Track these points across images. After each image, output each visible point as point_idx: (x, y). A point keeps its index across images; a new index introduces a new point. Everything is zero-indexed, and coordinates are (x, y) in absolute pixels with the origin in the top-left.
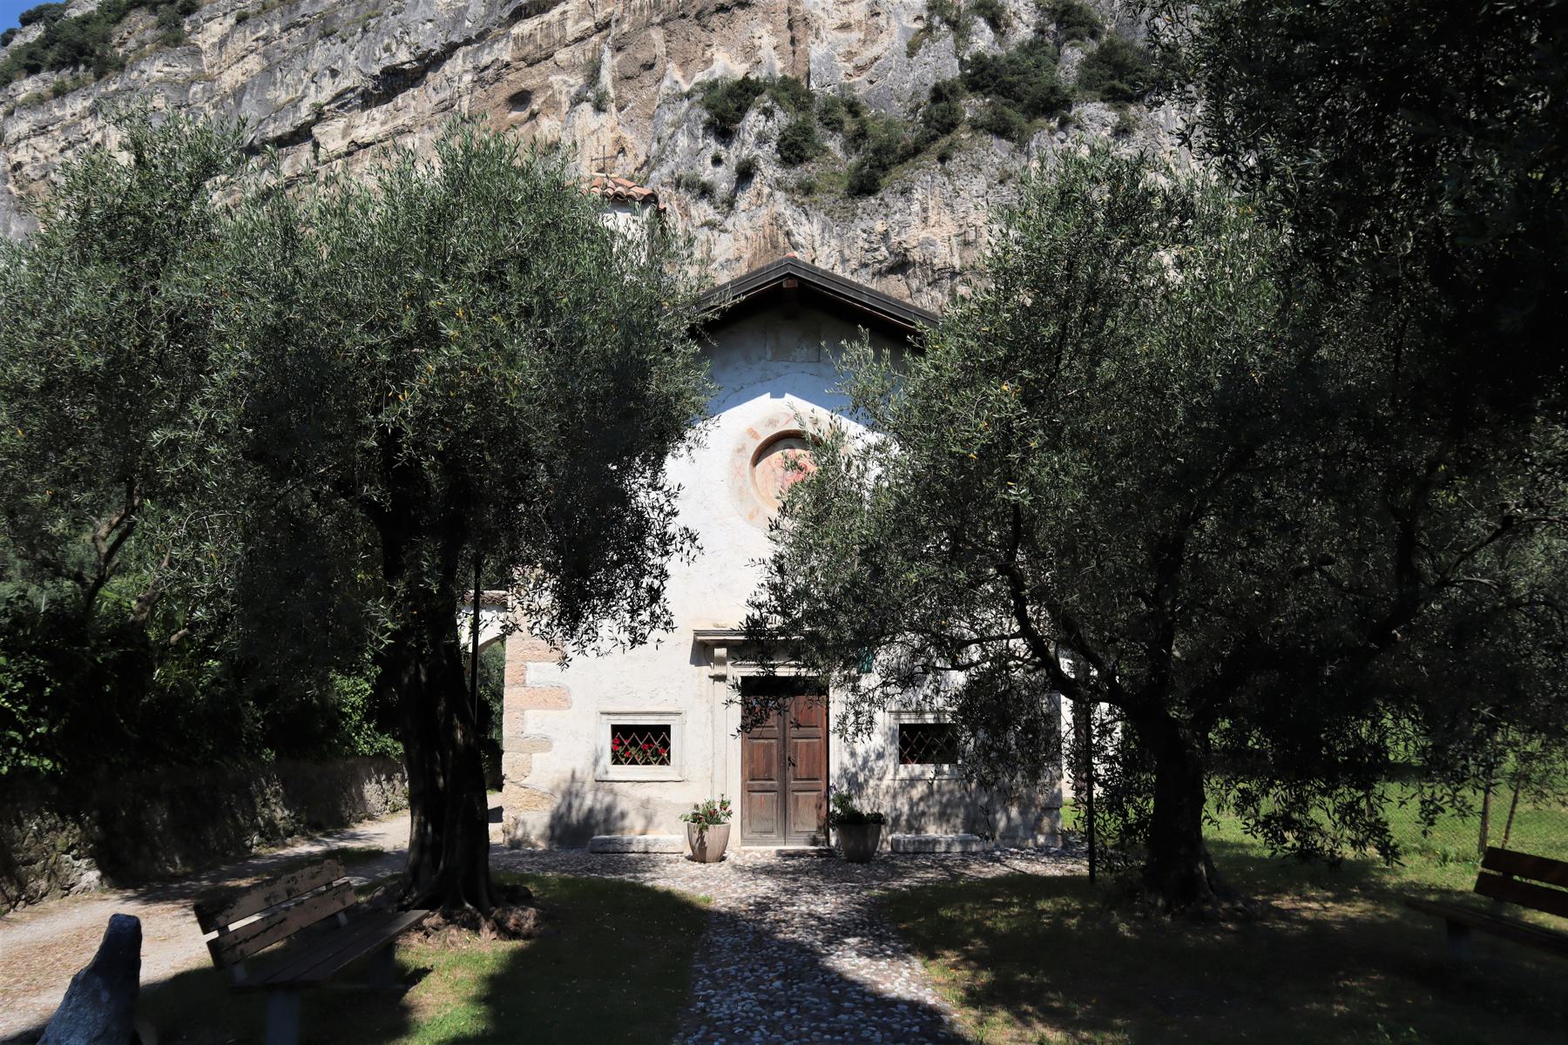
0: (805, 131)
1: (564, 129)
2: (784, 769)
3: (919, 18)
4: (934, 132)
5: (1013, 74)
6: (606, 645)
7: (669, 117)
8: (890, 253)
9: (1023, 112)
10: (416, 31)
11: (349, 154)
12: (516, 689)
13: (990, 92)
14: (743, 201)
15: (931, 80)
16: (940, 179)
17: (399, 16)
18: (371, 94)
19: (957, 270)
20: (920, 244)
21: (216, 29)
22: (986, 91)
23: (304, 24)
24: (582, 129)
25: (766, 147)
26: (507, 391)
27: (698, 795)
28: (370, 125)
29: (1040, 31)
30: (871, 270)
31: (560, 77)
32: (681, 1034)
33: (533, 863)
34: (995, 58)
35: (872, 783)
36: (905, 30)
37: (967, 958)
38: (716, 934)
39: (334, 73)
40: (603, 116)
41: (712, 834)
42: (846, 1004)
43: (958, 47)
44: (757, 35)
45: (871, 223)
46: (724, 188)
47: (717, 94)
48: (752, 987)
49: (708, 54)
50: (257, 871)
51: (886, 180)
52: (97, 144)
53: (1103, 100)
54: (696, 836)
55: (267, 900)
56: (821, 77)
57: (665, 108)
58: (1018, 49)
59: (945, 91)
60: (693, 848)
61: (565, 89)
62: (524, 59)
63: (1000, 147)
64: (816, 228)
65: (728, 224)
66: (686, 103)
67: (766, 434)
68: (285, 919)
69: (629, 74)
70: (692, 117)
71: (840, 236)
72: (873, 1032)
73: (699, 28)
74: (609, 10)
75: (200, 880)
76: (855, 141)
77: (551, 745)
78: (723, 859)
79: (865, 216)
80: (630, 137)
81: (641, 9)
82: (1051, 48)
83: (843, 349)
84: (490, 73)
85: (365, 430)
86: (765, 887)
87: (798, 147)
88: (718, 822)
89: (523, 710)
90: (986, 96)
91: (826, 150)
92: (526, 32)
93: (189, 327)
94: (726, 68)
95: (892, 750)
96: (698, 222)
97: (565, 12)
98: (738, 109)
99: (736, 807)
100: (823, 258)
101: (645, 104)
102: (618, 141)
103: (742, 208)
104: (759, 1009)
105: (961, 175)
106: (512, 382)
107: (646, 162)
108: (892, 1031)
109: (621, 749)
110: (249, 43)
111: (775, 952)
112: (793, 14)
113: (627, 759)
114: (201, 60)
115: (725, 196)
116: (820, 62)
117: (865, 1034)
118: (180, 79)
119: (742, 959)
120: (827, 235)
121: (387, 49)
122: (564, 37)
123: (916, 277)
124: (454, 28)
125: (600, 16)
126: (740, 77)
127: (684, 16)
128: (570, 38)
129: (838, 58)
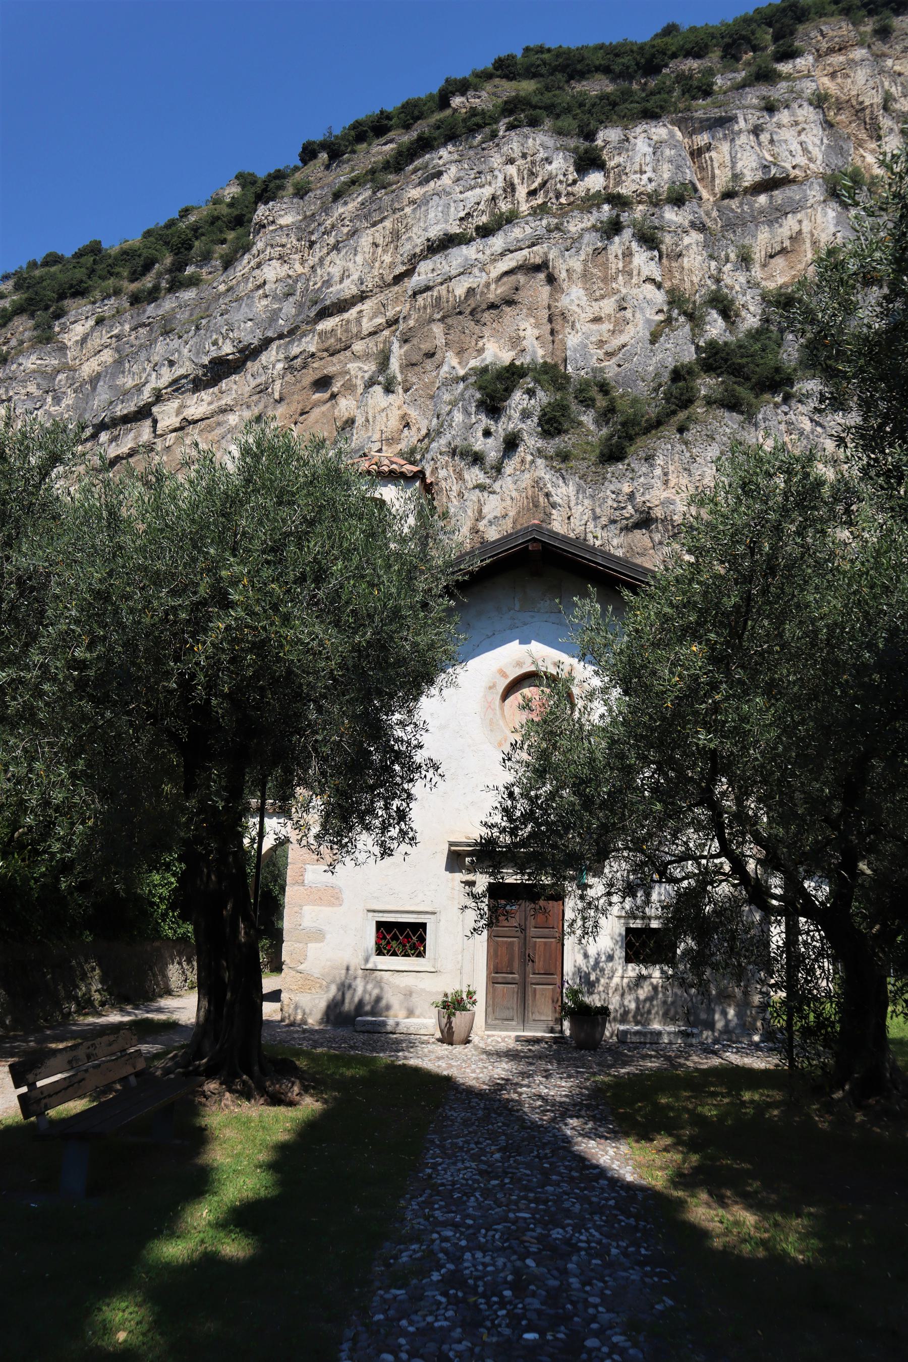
0: (562, 408)
1: (359, 407)
2: (524, 964)
3: (660, 311)
4: (673, 407)
5: (742, 357)
6: (362, 857)
7: (447, 397)
8: (636, 511)
9: (751, 389)
10: (239, 328)
11: (181, 428)
12: (296, 888)
13: (722, 373)
14: (509, 467)
15: (671, 363)
16: (679, 447)
17: (225, 317)
18: (201, 380)
20: (662, 503)
21: (79, 330)
22: (719, 371)
23: (149, 324)
24: (374, 408)
25: (529, 422)
26: (281, 646)
27: (449, 985)
29: (766, 321)
30: (619, 526)
31: (356, 365)
32: (408, 1196)
33: (304, 1039)
34: (726, 343)
35: (602, 981)
36: (648, 321)
37: (679, 1142)
38: (451, 1109)
39: (171, 363)
40: (392, 397)
41: (459, 1020)
42: (554, 1177)
43: (694, 335)
44: (522, 328)
45: (619, 485)
46: (493, 456)
47: (488, 377)
48: (475, 1158)
49: (480, 344)
50: (74, 1035)
51: (632, 449)
54: (445, 1021)
55: (70, 1062)
56: (577, 362)
57: (443, 389)
58: (746, 336)
59: (683, 372)
60: (442, 1032)
61: (360, 374)
62: (326, 350)
63: (731, 419)
64: (571, 490)
65: (496, 486)
66: (461, 385)
68: (83, 1079)
69: (414, 361)
70: (466, 396)
71: (592, 497)
72: (574, 1203)
73: (473, 323)
74: (398, 309)
75: (28, 1042)
76: (606, 415)
77: (324, 937)
78: (467, 1041)
79: (614, 479)
80: (413, 414)
81: (425, 308)
82: (775, 334)
83: (576, 605)
84: (298, 362)
85: (168, 674)
86: (502, 1070)
87: (556, 422)
88: (465, 1009)
89: (301, 906)
90: (719, 375)
91: (580, 424)
92: (329, 328)
93: (32, 589)
94: (495, 356)
95: (620, 954)
96: (470, 485)
97: (361, 311)
98: (506, 390)
99: (481, 997)
101: (427, 386)
102: (404, 416)
103: (508, 473)
104: (477, 1177)
105: (697, 444)
106: (285, 638)
107: (427, 435)
108: (591, 1203)
109: (383, 942)
110: (105, 340)
111: (499, 1127)
112: (553, 310)
113: (389, 951)
114: (66, 354)
115: (494, 463)
116: (575, 350)
117: (566, 1205)
118: (49, 369)
119: (470, 1132)
120: (581, 496)
121: (215, 343)
122: (360, 332)
123: (658, 531)
124: (270, 325)
125: (390, 314)
126: (507, 362)
127: (460, 313)
129: (591, 346)
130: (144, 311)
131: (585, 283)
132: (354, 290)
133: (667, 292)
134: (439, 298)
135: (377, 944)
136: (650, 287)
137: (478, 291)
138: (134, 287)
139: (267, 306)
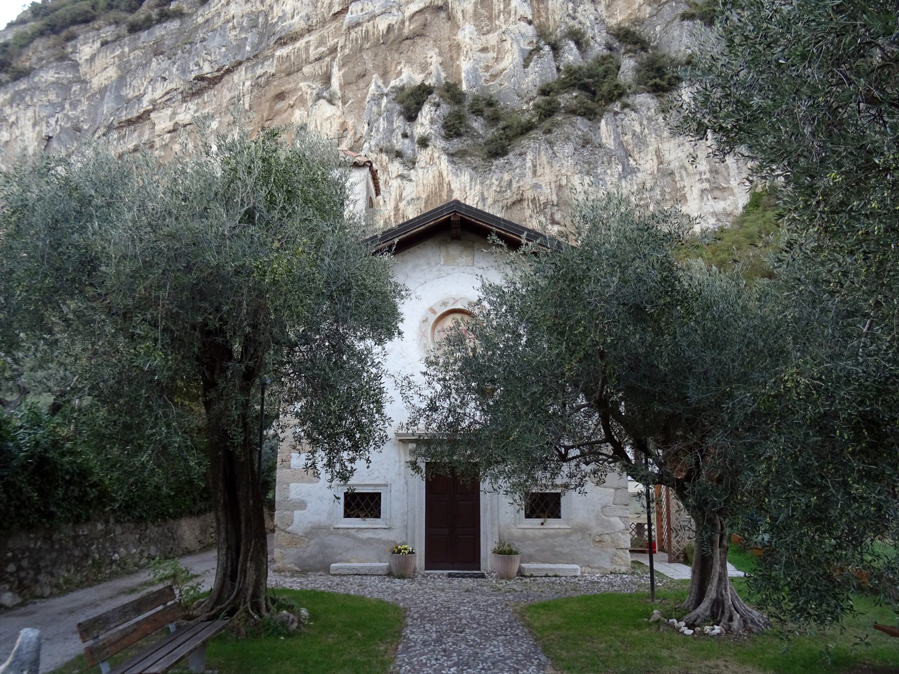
0: (460, 117)
12: (284, 470)
17: (204, 43)
19: (555, 203)
28: (186, 114)
38: (412, 633)
44: (429, 56)
49: (399, 68)
52: (13, 123)
53: (649, 92)
61: (309, 91)
67: (441, 311)
77: (306, 506)
89: (288, 484)
92: (285, 55)
94: (410, 77)
100: (471, 197)
114: (78, 70)
118: (65, 82)
121: (197, 64)
122: (308, 57)
124: (239, 51)
128: (312, 58)
130: (139, 38)
131: (475, 20)
132: (303, 25)
133: (536, 28)
134: (367, 31)
135: (345, 512)
136: (523, 24)
137: (396, 27)
138: (131, 18)
139: (236, 36)
